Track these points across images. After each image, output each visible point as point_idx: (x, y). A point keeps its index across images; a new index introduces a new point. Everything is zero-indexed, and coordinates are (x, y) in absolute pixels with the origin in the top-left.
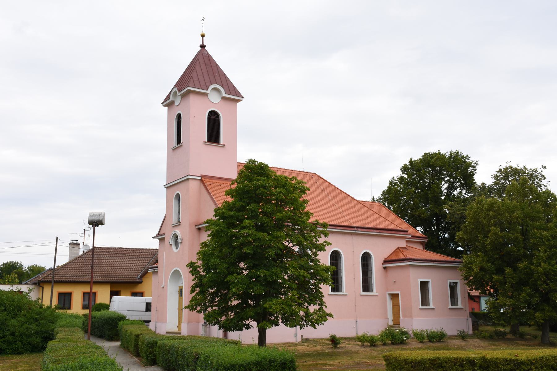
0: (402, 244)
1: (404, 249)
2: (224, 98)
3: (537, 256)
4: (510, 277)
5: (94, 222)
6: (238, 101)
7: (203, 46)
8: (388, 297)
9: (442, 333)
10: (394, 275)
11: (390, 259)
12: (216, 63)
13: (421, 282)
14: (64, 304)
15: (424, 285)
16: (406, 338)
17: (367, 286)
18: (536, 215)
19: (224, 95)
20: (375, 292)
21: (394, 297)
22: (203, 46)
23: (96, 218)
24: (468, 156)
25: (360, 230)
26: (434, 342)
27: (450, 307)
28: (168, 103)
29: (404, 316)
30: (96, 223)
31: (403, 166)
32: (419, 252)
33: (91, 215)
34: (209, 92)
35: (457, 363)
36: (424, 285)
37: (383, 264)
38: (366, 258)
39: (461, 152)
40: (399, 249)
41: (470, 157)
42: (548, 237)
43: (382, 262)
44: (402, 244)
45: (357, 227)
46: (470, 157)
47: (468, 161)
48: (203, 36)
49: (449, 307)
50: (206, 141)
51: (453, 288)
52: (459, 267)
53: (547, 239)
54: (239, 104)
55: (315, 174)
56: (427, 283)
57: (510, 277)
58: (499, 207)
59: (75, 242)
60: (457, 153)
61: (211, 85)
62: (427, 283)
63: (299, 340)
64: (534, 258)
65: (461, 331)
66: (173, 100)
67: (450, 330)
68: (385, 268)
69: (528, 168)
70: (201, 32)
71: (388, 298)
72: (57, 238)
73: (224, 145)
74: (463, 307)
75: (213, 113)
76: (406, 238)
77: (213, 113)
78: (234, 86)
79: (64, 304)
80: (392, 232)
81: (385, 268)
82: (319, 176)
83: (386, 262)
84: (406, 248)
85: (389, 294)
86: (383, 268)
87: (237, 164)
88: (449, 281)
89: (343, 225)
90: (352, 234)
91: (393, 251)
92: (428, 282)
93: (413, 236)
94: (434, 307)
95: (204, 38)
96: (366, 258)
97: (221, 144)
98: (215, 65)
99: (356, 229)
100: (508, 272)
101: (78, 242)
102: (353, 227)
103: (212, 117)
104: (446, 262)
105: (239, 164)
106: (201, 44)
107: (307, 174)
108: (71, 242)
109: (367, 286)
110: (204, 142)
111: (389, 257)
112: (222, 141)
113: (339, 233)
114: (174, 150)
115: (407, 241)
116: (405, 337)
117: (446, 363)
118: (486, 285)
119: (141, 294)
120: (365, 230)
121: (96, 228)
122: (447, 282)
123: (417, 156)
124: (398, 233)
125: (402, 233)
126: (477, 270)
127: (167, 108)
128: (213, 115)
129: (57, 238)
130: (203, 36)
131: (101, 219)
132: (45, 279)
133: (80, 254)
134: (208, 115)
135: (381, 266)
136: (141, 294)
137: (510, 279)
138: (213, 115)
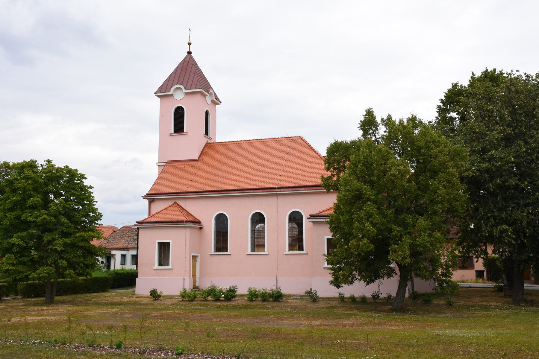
2: (186, 94)
7: (189, 53)
9: (279, 292)
11: (320, 214)
22: (189, 53)
31: (497, 72)
45: (278, 188)
48: (190, 44)
61: (182, 85)
70: (188, 41)
77: (177, 110)
88: (326, 238)
89: (237, 189)
90: (277, 195)
95: (190, 46)
96: (258, 218)
102: (182, 193)
110: (170, 134)
113: (297, 194)
118: (82, 224)
119: (123, 264)
120: (290, 189)
128: (178, 110)
130: (190, 44)
133: (534, 280)
136: (123, 264)
138: (178, 110)
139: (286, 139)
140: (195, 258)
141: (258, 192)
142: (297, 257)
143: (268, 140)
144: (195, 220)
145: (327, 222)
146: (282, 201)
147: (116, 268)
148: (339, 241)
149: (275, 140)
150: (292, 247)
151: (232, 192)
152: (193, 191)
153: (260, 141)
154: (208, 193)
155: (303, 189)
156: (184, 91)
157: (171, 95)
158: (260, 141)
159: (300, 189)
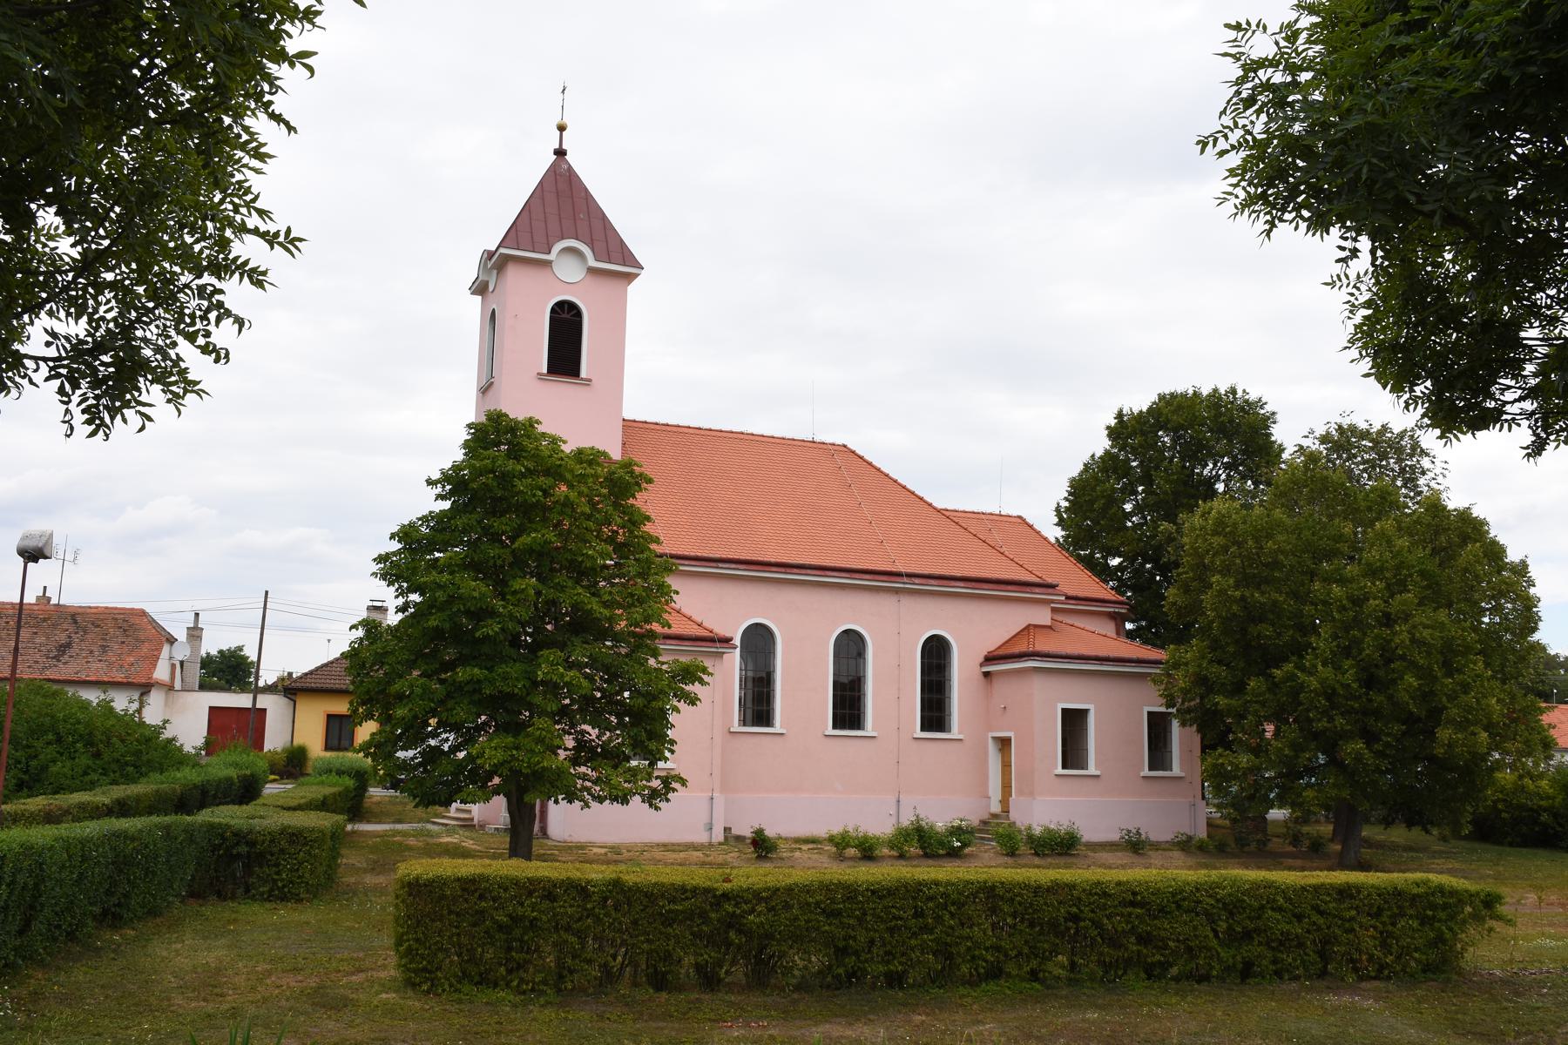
0: (1042, 616)
1: (1045, 631)
3: (1314, 649)
4: (1256, 702)
5: (27, 552)
6: (630, 277)
7: (560, 153)
8: (991, 743)
10: (1005, 691)
11: (1001, 652)
12: (586, 190)
13: (1064, 710)
14: (340, 739)
15: (1074, 722)
16: (959, 844)
17: (935, 715)
18: (1327, 545)
19: (592, 263)
20: (955, 731)
21: (1004, 743)
22: (560, 153)
23: (31, 544)
24: (1260, 400)
25: (917, 581)
26: (1044, 855)
27: (1146, 772)
28: (480, 289)
29: (1020, 793)
30: (32, 554)
32: (1099, 636)
33: (25, 537)
34: (552, 257)
35: (535, 891)
36: (1074, 722)
37: (982, 665)
38: (936, 654)
39: (1244, 391)
40: (1028, 629)
41: (1266, 403)
42: (1341, 601)
43: (981, 659)
44: (1042, 616)
46: (1266, 403)
47: (1262, 412)
48: (562, 128)
49: (1142, 774)
50: (545, 370)
51: (1158, 728)
52: (1150, 673)
53: (1339, 606)
54: (633, 288)
55: (845, 446)
56: (1083, 713)
57: (1256, 702)
58: (1235, 524)
59: (379, 604)
60: (1233, 391)
61: (563, 239)
62: (1083, 713)
63: (718, 836)
64: (1307, 654)
65: (1129, 831)
66: (486, 279)
67: (1158, 829)
68: (987, 675)
69: (472, 418)
70: (557, 120)
71: (992, 748)
72: (267, 593)
73: (590, 380)
74: (1183, 774)
75: (566, 306)
76: (1053, 601)
78: (622, 240)
79: (340, 739)
80: (1010, 588)
81: (987, 675)
82: (853, 452)
83: (990, 659)
84: (1050, 627)
85: (994, 738)
86: (982, 677)
87: (621, 423)
88: (1146, 709)
90: (897, 591)
91: (1014, 633)
92: (1084, 712)
93: (1068, 598)
94: (1098, 773)
96: (936, 654)
97: (582, 379)
98: (583, 194)
99: (905, 580)
100: (1253, 689)
101: (385, 604)
102: (899, 574)
103: (563, 316)
104: (1139, 662)
105: (625, 423)
106: (557, 147)
107: (822, 446)
108: (371, 604)
109: (935, 715)
111: (999, 648)
112: (583, 374)
114: (484, 393)
115: (1054, 610)
116: (958, 841)
117: (506, 890)
120: (932, 582)
121: (30, 565)
122: (1142, 710)
123: (1140, 401)
124: (1028, 589)
125: (1037, 590)
126: (1185, 682)
127: (480, 297)
129: (267, 593)
130: (562, 128)
131: (40, 545)
132: (298, 684)
134: (553, 310)
135: (977, 671)
137: (1257, 706)
139: (811, 445)
140: (1004, 743)
141: (717, 568)
142: (848, 744)
143: (778, 441)
144: (706, 634)
145: (1155, 680)
146: (909, 605)
147: (295, 743)
148: (397, 687)
149: (679, 429)
150: (839, 722)
151: (795, 571)
152: (692, 554)
153: (747, 437)
154: (733, 566)
155: (961, 584)
156: (592, 263)
157: (548, 264)
158: (747, 437)
159: (953, 583)
